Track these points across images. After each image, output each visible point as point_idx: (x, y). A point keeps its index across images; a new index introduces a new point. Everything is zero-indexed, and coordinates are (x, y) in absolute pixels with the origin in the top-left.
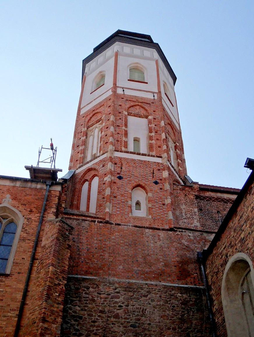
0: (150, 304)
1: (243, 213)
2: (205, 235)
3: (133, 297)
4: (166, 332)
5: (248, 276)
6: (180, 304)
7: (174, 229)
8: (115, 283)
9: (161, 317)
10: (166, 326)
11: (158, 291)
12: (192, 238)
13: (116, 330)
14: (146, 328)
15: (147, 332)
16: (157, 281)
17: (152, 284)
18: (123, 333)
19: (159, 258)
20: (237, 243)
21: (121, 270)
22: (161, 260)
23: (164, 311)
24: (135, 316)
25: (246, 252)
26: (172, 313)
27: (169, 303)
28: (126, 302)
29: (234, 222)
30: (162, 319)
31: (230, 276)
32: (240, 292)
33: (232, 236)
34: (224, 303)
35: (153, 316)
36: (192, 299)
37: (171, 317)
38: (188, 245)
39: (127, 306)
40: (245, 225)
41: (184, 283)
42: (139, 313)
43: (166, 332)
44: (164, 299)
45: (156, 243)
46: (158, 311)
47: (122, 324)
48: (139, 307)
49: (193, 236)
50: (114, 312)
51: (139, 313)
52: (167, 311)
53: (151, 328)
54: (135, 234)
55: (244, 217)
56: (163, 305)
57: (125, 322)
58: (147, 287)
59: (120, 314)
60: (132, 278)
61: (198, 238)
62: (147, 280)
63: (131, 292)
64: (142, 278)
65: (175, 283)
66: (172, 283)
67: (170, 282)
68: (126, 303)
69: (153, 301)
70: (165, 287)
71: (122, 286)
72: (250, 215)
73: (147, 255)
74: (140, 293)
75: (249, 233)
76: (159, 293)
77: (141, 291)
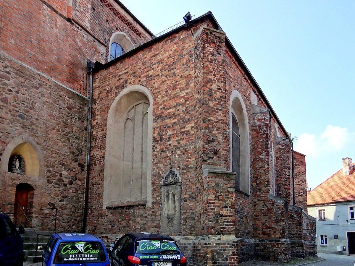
0: (39, 98)
1: (159, 54)
2: (97, 43)
3: (24, 84)
4: (51, 131)
5: (137, 107)
6: (66, 107)
7: (72, 21)
8: (6, 59)
9: (49, 116)
10: (52, 125)
11: (49, 87)
12: (85, 40)
13: (4, 116)
14: (34, 122)
15: (34, 127)
16: (48, 75)
17: (44, 77)
18: (10, 121)
19: (53, 48)
20: (142, 76)
21: (12, 45)
22: (55, 52)
23: (52, 110)
24: (24, 107)
25: (150, 89)
26: (59, 115)
27: (57, 103)
28: (17, 88)
29: (145, 56)
30: (49, 117)
31: (123, 101)
32: (125, 116)
33: (139, 67)
34: (110, 122)
35: (42, 112)
36: (76, 106)
37: (57, 118)
38: (81, 46)
39: (17, 92)
40: (157, 65)
41: (72, 87)
42: (28, 105)
43: (51, 131)
44: (54, 97)
45: (52, 28)
46: (47, 108)
47: (10, 111)
48: (30, 98)
49: (87, 39)
50: (3, 94)
51: (28, 105)
52: (54, 111)
53: (38, 124)
54: (32, 5)
55: (159, 58)
56: (52, 104)
57: (13, 110)
58: (39, 78)
59: (9, 100)
60: (24, 60)
61: (90, 44)
62: (39, 70)
63: (23, 78)
64: (34, 65)
65: (64, 84)
66: (61, 83)
67: (60, 81)
68: (16, 89)
69: (43, 96)
70: (56, 85)
71: (13, 66)
72: (165, 60)
73: (41, 39)
74: (32, 83)
75: (159, 75)
76: (50, 89)
77: (32, 80)
